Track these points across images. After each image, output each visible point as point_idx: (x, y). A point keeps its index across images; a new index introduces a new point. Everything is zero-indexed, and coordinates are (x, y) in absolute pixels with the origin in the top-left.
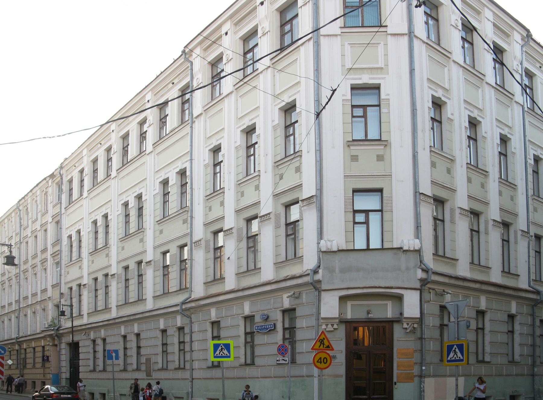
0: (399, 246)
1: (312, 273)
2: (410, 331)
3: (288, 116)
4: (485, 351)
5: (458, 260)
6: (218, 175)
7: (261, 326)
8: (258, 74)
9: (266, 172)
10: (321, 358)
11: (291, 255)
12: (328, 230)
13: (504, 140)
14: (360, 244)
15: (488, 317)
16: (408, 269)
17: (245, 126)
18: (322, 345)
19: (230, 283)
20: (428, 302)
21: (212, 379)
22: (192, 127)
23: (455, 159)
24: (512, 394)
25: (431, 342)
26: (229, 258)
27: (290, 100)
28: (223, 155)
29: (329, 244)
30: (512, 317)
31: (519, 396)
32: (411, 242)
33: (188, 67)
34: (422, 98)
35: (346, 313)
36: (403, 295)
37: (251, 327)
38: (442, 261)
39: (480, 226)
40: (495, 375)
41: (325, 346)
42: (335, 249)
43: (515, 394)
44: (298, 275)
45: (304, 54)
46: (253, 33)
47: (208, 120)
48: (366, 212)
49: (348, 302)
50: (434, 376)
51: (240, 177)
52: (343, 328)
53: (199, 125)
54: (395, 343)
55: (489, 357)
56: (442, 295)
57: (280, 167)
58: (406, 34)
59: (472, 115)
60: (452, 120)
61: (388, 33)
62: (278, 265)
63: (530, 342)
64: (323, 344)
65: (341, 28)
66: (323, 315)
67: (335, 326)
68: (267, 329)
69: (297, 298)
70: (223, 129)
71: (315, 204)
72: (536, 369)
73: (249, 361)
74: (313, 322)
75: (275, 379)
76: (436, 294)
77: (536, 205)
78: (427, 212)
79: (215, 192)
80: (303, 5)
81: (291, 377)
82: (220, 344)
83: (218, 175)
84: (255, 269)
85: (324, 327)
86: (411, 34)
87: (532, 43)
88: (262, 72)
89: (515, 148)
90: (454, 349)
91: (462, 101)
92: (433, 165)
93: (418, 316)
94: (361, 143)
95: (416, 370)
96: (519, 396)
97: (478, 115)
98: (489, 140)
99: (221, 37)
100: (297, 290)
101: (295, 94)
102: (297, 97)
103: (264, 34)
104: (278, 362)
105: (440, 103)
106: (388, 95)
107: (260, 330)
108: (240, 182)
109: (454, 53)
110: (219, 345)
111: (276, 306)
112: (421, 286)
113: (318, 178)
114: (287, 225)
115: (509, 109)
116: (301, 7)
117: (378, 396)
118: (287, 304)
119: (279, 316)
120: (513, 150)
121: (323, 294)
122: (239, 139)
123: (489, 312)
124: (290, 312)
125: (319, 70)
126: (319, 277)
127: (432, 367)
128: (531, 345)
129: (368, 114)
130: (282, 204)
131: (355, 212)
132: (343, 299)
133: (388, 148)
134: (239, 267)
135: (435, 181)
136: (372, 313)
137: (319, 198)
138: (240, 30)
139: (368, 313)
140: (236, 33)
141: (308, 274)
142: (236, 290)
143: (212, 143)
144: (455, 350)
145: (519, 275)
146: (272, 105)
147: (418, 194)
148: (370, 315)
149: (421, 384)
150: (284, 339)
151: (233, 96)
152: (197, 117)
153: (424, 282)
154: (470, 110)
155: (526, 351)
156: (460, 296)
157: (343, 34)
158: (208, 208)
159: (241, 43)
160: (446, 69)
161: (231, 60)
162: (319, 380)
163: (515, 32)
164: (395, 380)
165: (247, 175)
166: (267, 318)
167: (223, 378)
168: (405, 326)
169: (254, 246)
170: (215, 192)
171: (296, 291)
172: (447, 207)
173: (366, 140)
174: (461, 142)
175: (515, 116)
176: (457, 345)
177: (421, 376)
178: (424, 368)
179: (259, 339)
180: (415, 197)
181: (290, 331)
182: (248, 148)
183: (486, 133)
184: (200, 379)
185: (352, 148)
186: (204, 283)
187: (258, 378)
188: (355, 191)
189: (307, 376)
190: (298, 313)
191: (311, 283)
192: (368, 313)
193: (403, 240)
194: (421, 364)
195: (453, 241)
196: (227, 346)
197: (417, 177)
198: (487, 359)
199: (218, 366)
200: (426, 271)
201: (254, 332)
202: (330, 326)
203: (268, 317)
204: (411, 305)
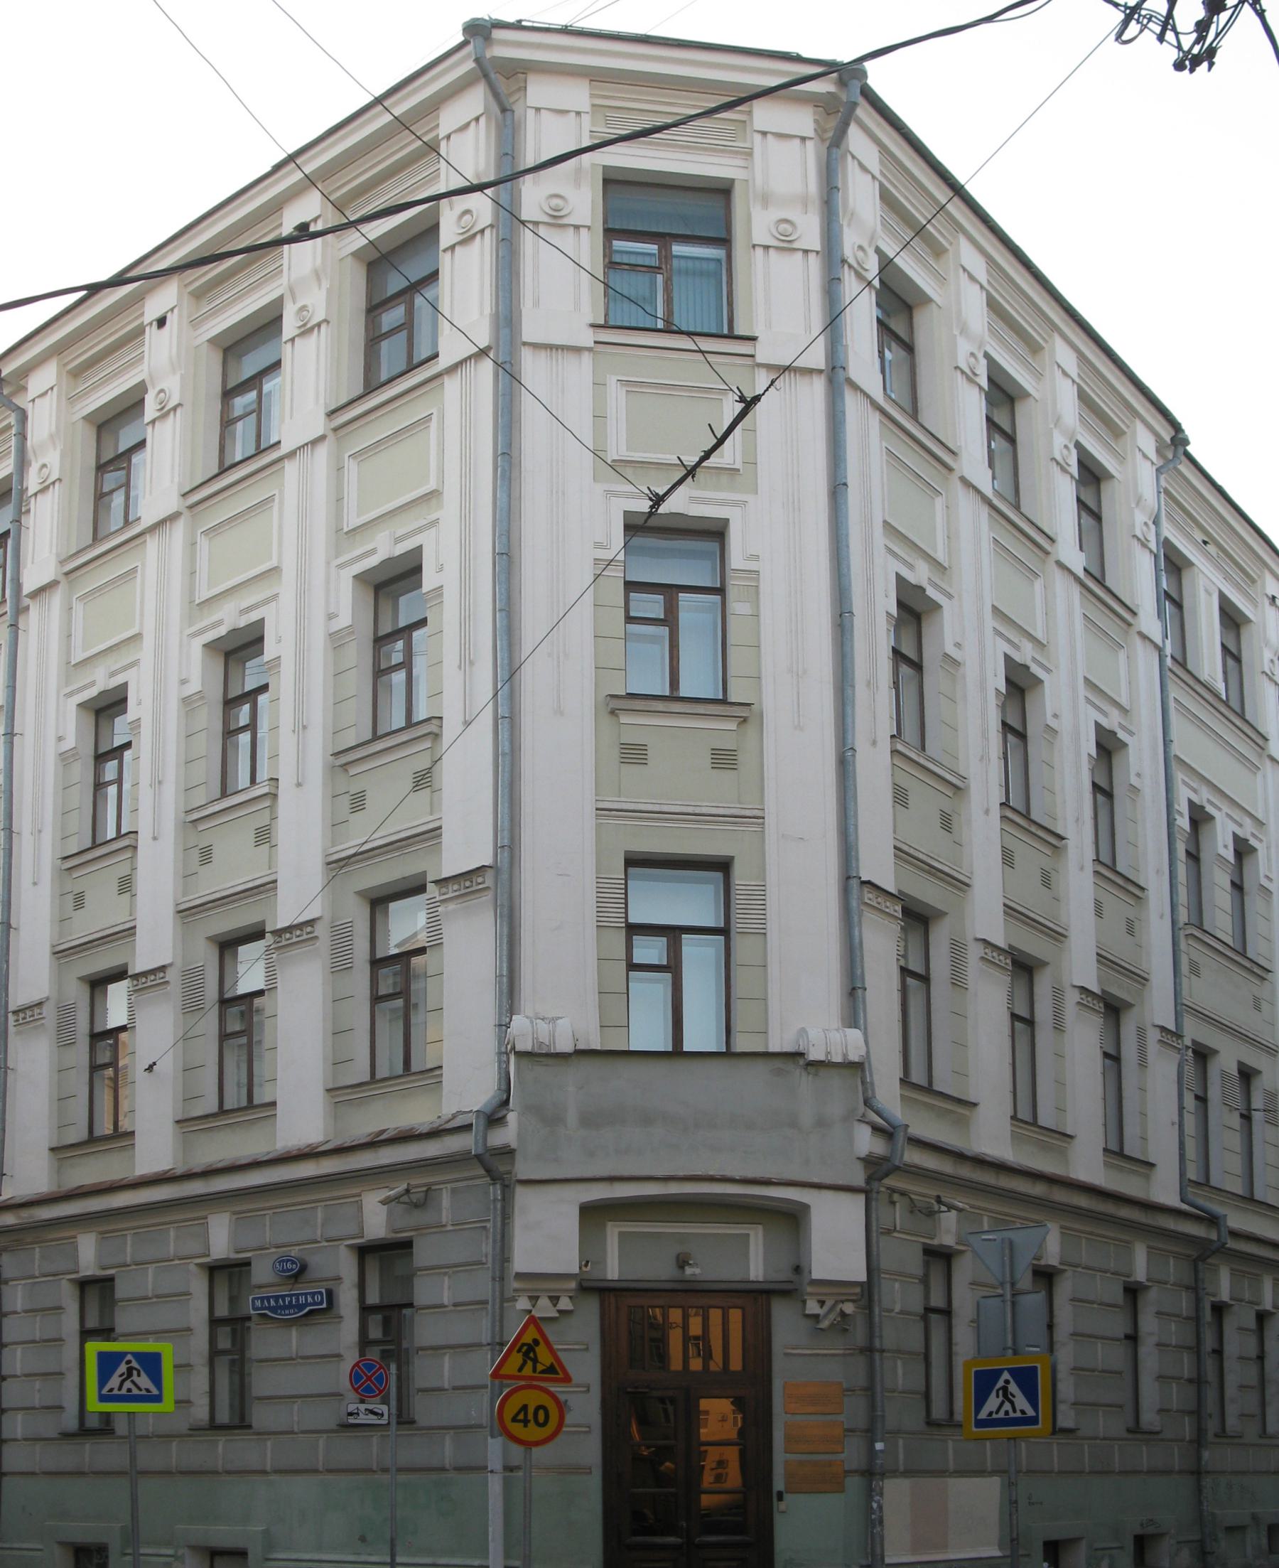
0: (788, 1048)
1: (482, 1121)
2: (832, 1325)
3: (386, 608)
4: (1060, 1396)
5: (975, 1105)
6: (112, 790)
7: (276, 1298)
8: (281, 459)
9: (299, 785)
10: (525, 1408)
11: (389, 1061)
12: (526, 986)
13: (1108, 748)
14: (649, 1033)
15: (1064, 1289)
16: (822, 1123)
17: (222, 631)
18: (530, 1364)
19: (155, 1148)
20: (888, 1232)
21: (80, 1473)
22: (14, 626)
23: (968, 787)
24: (1139, 1531)
25: (899, 1363)
26: (150, 1068)
27: (400, 549)
28: (136, 724)
29: (543, 1027)
30: (1133, 1292)
31: (1157, 1537)
32: (836, 1037)
33: (9, 427)
34: (870, 581)
35: (602, 1261)
36: (806, 1208)
37: (233, 1300)
38: (925, 1104)
39: (1037, 1006)
40: (1090, 1472)
41: (540, 1367)
42: (565, 1046)
43: (1150, 1530)
44: (425, 1129)
45: (464, 404)
46: (266, 325)
47: (78, 608)
48: (673, 933)
49: (610, 1224)
50: (908, 1473)
51: (200, 797)
52: (591, 1307)
53: (43, 626)
54: (780, 1367)
55: (1072, 1413)
56: (931, 1214)
57: (353, 771)
58: (821, 371)
59: (1017, 657)
60: (956, 663)
61: (759, 359)
62: (341, 1095)
63: (1187, 1370)
64: (531, 1357)
65: (593, 326)
66: (521, 1262)
67: (565, 1304)
68: (301, 1307)
69: (416, 1206)
70: (137, 637)
71: (489, 897)
72: (1206, 1455)
73: (224, 1416)
74: (482, 1286)
75: (330, 1477)
76: (913, 1208)
77: (1195, 956)
78: (882, 944)
79: (100, 848)
80: (461, 243)
81: (399, 1470)
82: (124, 1354)
83: (112, 790)
84: (251, 1105)
85: (523, 1303)
86: (835, 375)
87: (1185, 468)
88: (291, 455)
89: (1138, 775)
90: (1000, 1383)
91: (988, 609)
92: (900, 797)
93: (863, 1277)
94: (660, 706)
95: (852, 1454)
96: (1157, 1537)
97: (1034, 659)
98: (1065, 739)
99: (139, 332)
100: (418, 1180)
101: (420, 530)
102: (426, 540)
103: (306, 331)
104: (352, 1420)
105: (918, 608)
106: (756, 558)
107: (273, 1309)
108: (196, 816)
109: (964, 456)
110: (118, 1357)
111: (333, 1233)
112: (869, 1180)
113: (503, 809)
114: (377, 963)
115: (1122, 655)
116: (452, 248)
117: (722, 1538)
118: (376, 1220)
119: (347, 1267)
120: (1134, 781)
121: (523, 1196)
122: (194, 671)
123: (1069, 1274)
124: (384, 1254)
125: (515, 453)
126: (506, 1135)
127: (901, 1442)
128: (1190, 1381)
129: (684, 617)
130: (360, 893)
131: (634, 930)
132: (593, 1214)
133: (751, 730)
134: (189, 1099)
135: (905, 848)
136: (696, 1265)
137: (505, 876)
138: (215, 312)
139: (682, 1262)
140: (195, 323)
141: (467, 1128)
142: (179, 1172)
143: (93, 684)
144: (1005, 1389)
145: (1152, 1165)
146: (328, 563)
147: (854, 883)
148: (689, 1271)
149: (870, 1497)
150: (365, 1342)
151: (179, 531)
152: (35, 594)
153: (876, 1168)
154: (1009, 641)
155: (1178, 1397)
156: (985, 1219)
157: (600, 348)
158: (70, 898)
159: (217, 358)
160: (939, 503)
161: (175, 409)
162: (507, 1486)
163: (1140, 427)
164: (779, 1484)
165: (224, 794)
166: (298, 1272)
167: (134, 1474)
168: (812, 1307)
169: (247, 1032)
170: (100, 848)
171: (413, 1182)
172: (940, 936)
173: (674, 698)
174: (985, 734)
175: (1137, 676)
176: (1011, 1371)
177: (871, 1473)
178: (879, 1446)
179: (266, 1342)
180: (845, 891)
181: (389, 1321)
182: (230, 703)
183: (1055, 716)
184: (33, 1473)
185: (625, 719)
186: (52, 1149)
187: (264, 1472)
188: (634, 861)
189: (458, 1469)
190: (424, 1253)
191: (477, 1156)
192: (682, 1262)
193: (803, 1031)
194: (870, 1433)
195: (960, 1045)
196: (151, 1363)
197: (852, 829)
198: (1066, 1418)
199: (105, 1427)
200: (886, 1132)
201: (249, 1318)
202: (544, 1302)
203: (303, 1268)
204: (837, 1241)
